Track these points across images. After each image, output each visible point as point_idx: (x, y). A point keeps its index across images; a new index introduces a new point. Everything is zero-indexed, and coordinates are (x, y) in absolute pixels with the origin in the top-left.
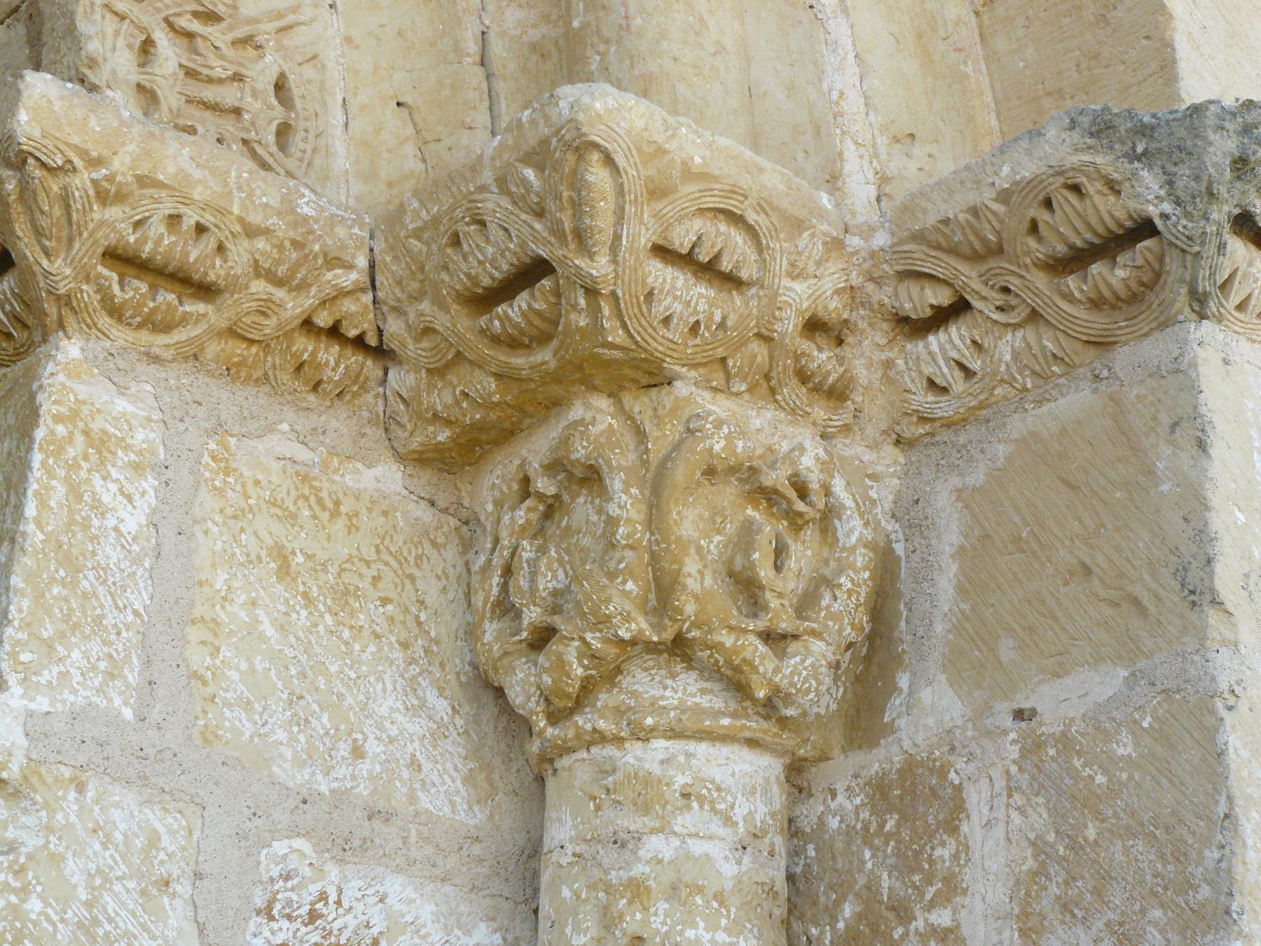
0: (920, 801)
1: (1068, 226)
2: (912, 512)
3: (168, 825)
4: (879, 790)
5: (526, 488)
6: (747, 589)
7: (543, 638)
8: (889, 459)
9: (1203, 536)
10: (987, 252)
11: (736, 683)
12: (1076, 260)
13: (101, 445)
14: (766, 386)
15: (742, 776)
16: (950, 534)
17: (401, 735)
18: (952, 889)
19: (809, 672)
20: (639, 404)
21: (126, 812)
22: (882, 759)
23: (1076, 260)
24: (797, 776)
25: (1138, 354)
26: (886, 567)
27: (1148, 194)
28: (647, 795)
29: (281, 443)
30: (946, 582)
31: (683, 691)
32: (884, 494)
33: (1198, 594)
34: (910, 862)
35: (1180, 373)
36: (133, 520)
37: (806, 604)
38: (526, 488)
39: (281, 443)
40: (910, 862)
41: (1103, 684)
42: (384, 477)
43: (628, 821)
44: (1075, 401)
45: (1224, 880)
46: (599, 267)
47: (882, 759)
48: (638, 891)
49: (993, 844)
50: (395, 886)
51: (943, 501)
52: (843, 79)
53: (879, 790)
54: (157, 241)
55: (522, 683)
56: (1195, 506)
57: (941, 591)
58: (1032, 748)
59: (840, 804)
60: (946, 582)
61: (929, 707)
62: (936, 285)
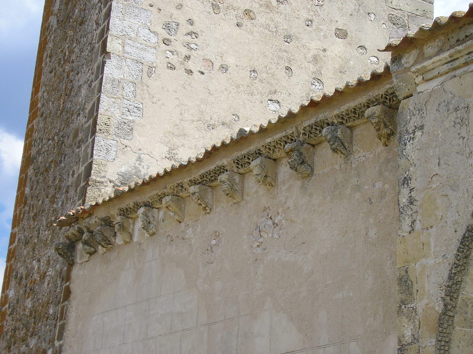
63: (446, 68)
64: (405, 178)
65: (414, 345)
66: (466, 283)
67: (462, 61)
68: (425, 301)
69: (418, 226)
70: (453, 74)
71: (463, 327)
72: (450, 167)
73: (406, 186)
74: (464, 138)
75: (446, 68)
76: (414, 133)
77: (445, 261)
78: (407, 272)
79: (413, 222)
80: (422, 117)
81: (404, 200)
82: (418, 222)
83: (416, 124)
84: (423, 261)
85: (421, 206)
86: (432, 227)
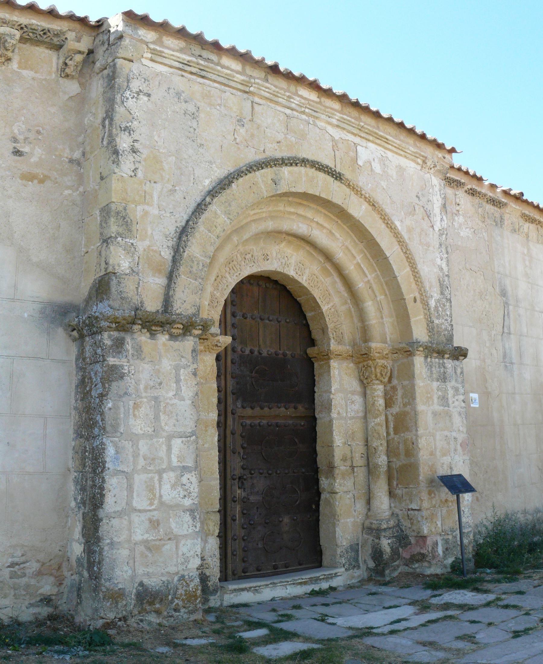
0: (394, 388)
1: (405, 350)
2: (393, 365)
3: (342, 395)
4: (391, 387)
5: (364, 366)
6: (382, 375)
7: (366, 378)
8: (391, 362)
9: (414, 373)
10: (399, 350)
11: (381, 381)
12: (406, 352)
13: (334, 368)
14: (383, 359)
15: (381, 387)
16: (396, 369)
17: (355, 385)
18: (397, 395)
19: (386, 380)
20: (374, 361)
21: (340, 395)
22: (391, 385)
23: (406, 352)
24: (385, 386)
25: (410, 358)
26: (391, 369)
27: (411, 349)
28: (375, 390)
29: (345, 364)
30: (396, 372)
31: (377, 382)
32: (391, 364)
33: (414, 377)
34: (394, 393)
35: (413, 361)
36: (337, 373)
37: (386, 375)
38: (364, 366)
39: (345, 364)
40: (394, 393)
41: (408, 382)
42: (352, 365)
43: (374, 392)
44: (405, 360)
45: (415, 397)
46: (372, 355)
47: (391, 385)
48: (375, 397)
49: (400, 392)
50: (356, 396)
51: (395, 365)
52: (387, 330)
53: (391, 387)
54: (339, 353)
55: (365, 381)
56: (414, 371)
57: (395, 373)
58: (403, 386)
59: (388, 388)
60: (396, 372)
61: (395, 382)
62: (395, 351)
63: (177, 64)
64: (127, 127)
65: (132, 277)
66: (192, 243)
67: (194, 70)
68: (147, 243)
69: (140, 174)
70: (180, 72)
71: (188, 277)
72: (180, 145)
73: (127, 134)
74: (195, 129)
75: (177, 64)
76: (138, 93)
77: (172, 217)
78: (125, 209)
79: (136, 169)
80: (147, 86)
81: (124, 145)
82: (139, 170)
83: (140, 88)
84: (146, 207)
85: (145, 160)
86: (155, 182)
